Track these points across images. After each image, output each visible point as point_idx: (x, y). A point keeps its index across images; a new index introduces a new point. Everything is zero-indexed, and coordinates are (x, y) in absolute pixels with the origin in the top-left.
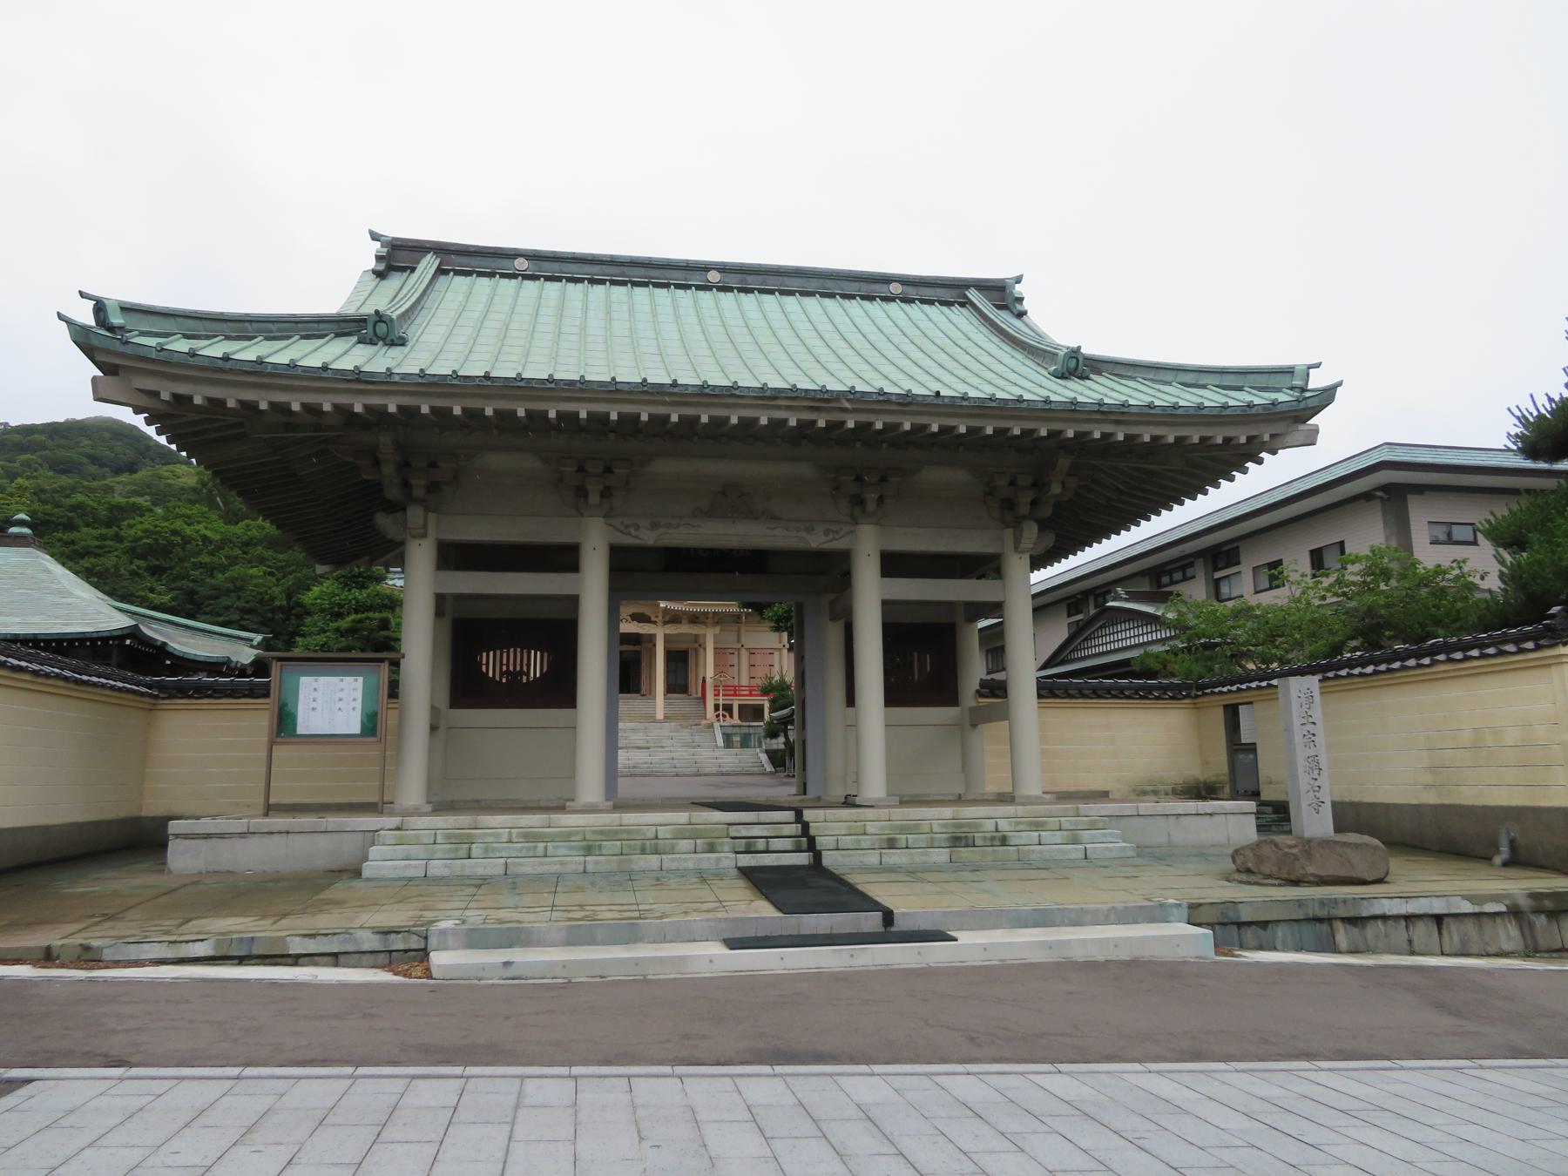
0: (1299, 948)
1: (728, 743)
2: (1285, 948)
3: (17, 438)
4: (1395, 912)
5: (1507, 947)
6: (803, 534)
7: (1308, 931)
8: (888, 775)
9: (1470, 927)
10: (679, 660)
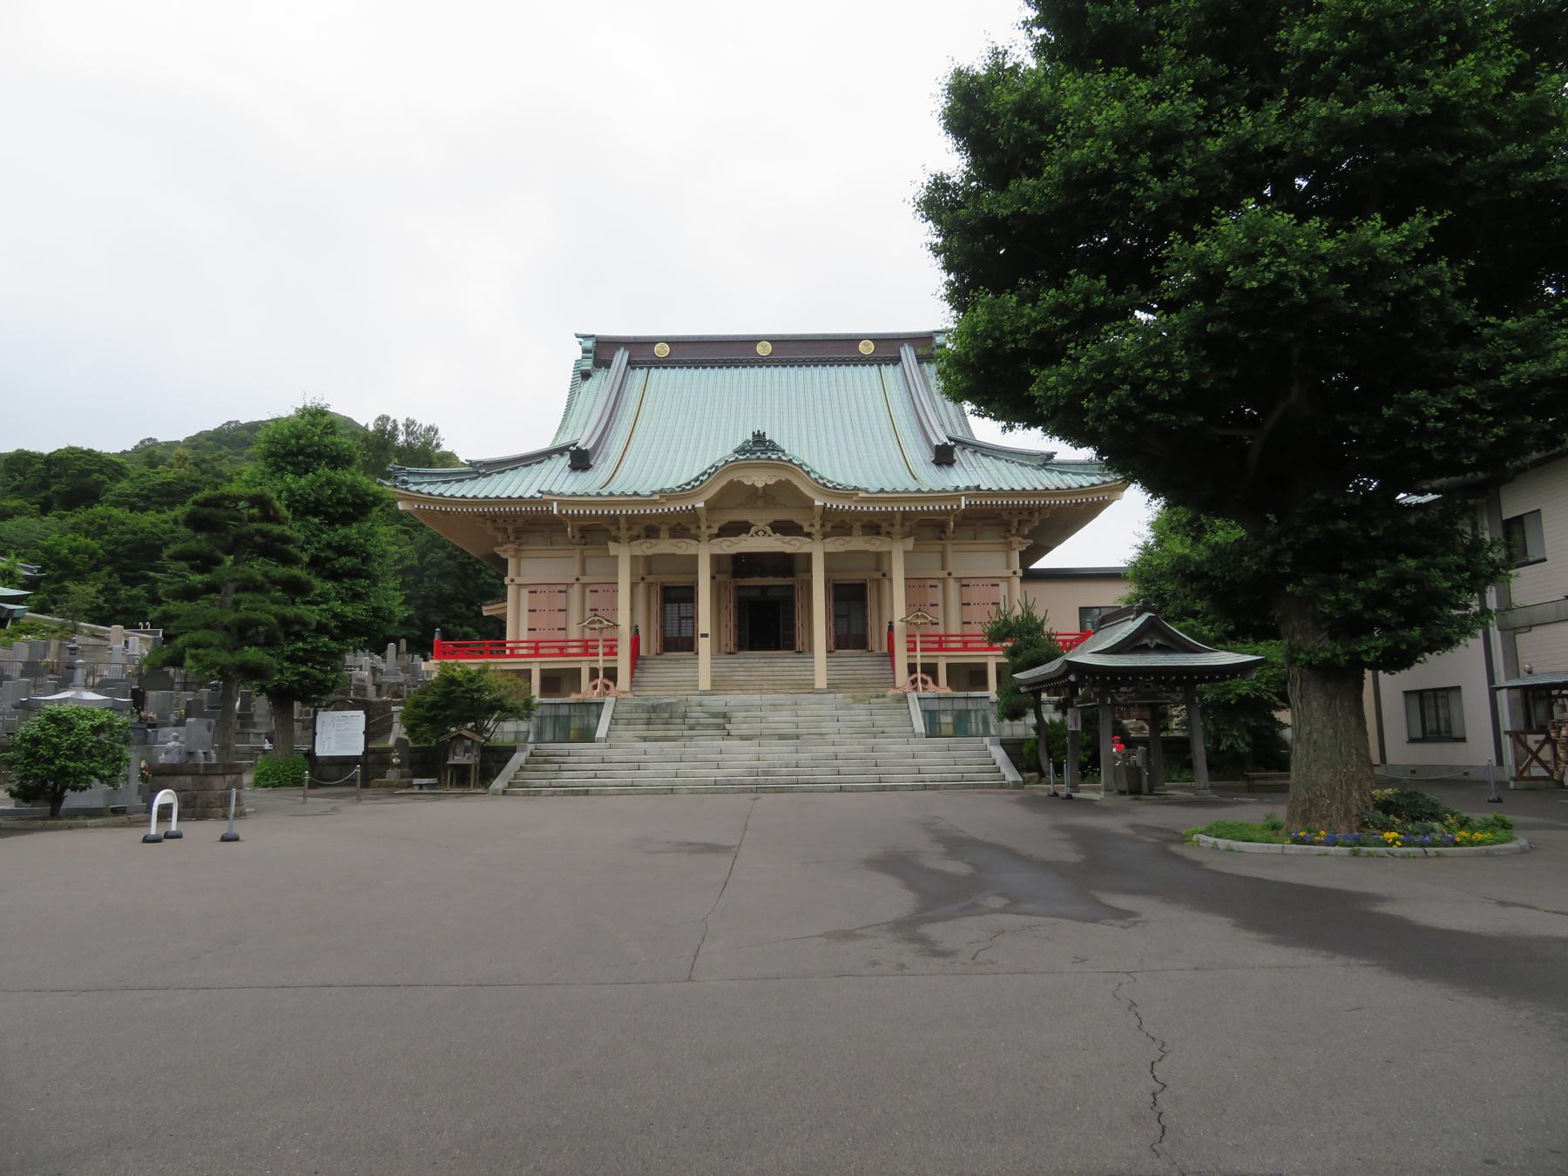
1: (933, 730)
3: (245, 433)
8: (778, 648)
10: (852, 600)
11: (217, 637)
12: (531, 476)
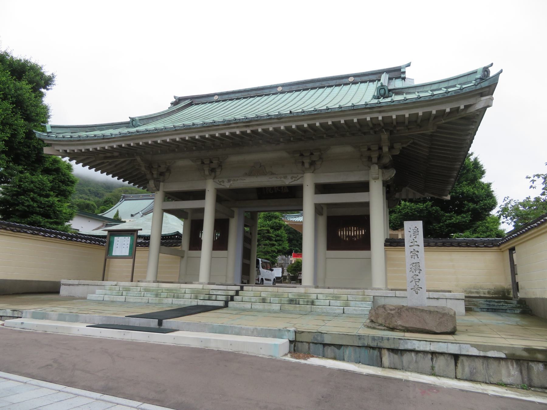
0: (358, 361)
2: (349, 361)
4: (421, 349)
5: (505, 380)
6: (283, 179)
7: (365, 353)
9: (479, 364)
11: (262, 254)
12: (335, 101)
